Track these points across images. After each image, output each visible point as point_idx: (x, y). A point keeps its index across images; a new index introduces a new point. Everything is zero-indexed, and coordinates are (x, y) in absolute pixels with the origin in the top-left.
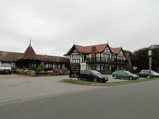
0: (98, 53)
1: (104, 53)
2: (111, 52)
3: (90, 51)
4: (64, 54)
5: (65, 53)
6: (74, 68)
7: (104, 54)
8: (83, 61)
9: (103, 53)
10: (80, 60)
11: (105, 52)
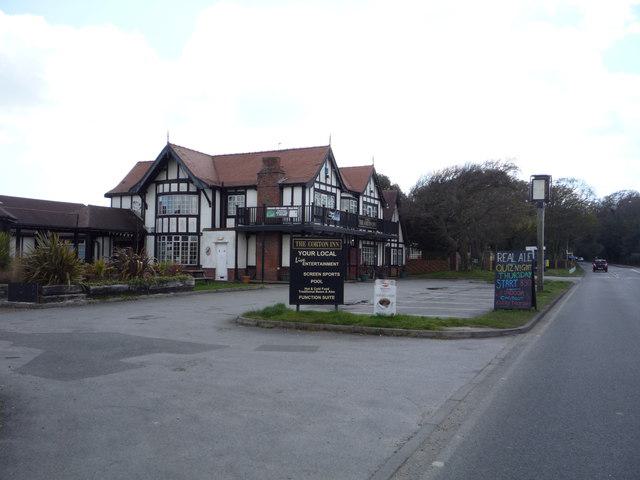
0: (293, 186)
1: (317, 186)
2: (341, 187)
3: (254, 180)
4: (107, 190)
5: (112, 184)
6: (313, 253)
7: (315, 190)
8: (218, 225)
9: (312, 189)
10: (198, 217)
11: (320, 183)
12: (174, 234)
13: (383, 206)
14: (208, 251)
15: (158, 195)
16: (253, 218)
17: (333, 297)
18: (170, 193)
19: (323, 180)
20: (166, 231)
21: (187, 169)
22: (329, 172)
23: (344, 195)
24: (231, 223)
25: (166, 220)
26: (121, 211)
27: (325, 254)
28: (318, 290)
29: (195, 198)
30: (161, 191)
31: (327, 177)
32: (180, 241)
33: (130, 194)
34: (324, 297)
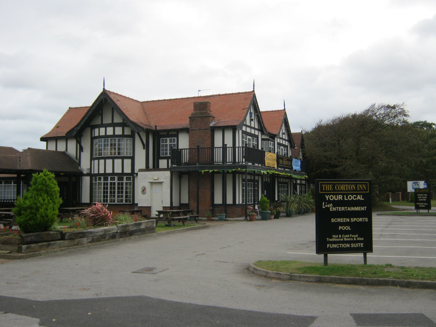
0: (223, 129)
2: (262, 129)
3: (186, 123)
6: (340, 197)
7: (243, 132)
8: (151, 166)
9: (240, 132)
10: (133, 159)
11: (247, 126)
12: (109, 174)
13: (292, 147)
14: (144, 191)
15: (93, 139)
16: (186, 158)
17: (362, 245)
18: (106, 136)
19: (248, 124)
20: (102, 171)
21: (121, 113)
22: (253, 115)
23: (264, 137)
24: (163, 163)
25: (102, 161)
26: (56, 152)
27: (352, 197)
28: (346, 238)
29: (129, 141)
30: (97, 134)
31: (251, 120)
32: (116, 181)
33: (67, 138)
34: (353, 245)
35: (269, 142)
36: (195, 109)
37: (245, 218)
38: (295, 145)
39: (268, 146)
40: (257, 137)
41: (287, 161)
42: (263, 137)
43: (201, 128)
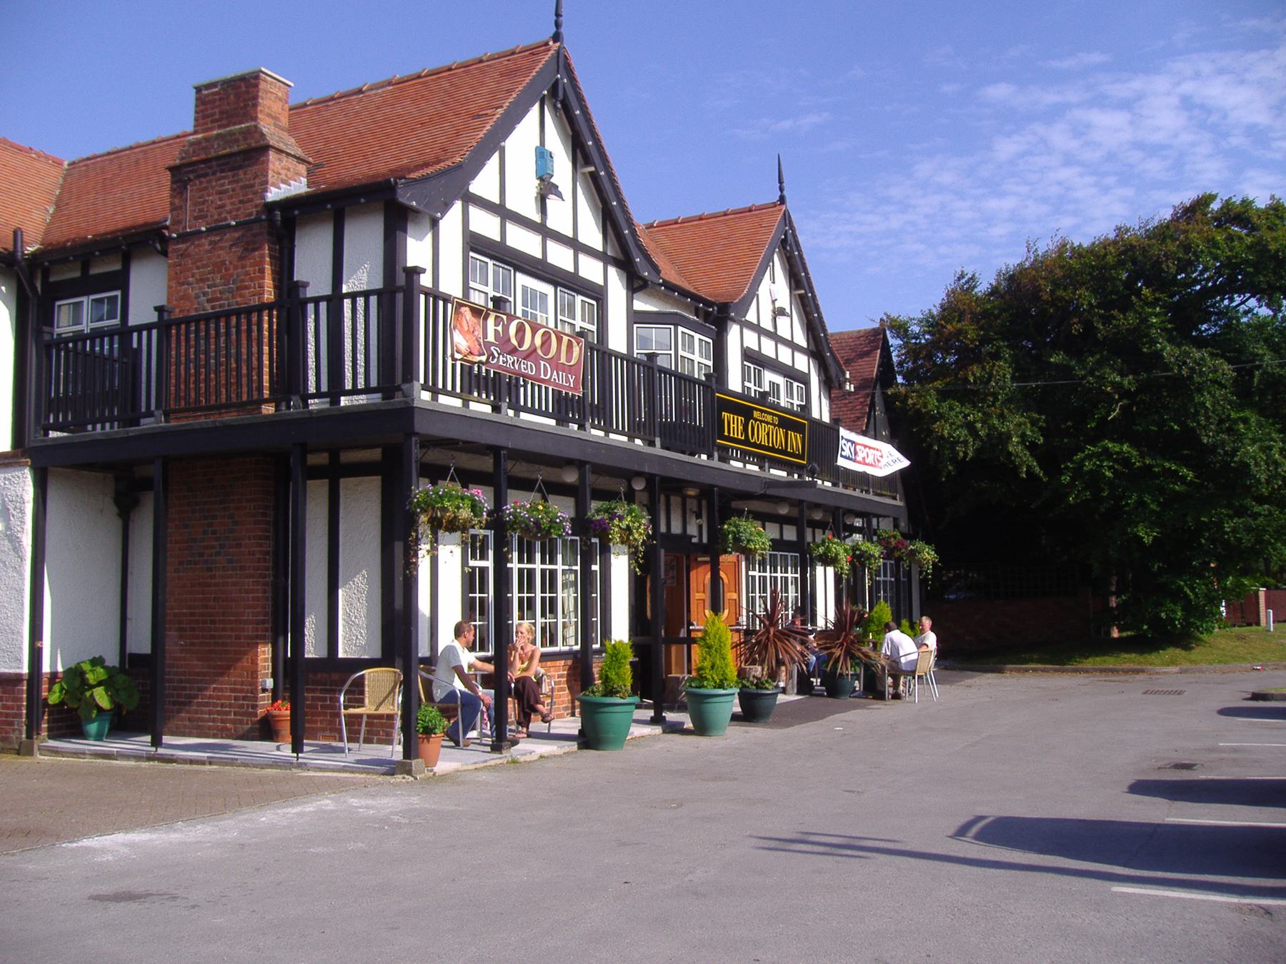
35: (681, 329)
36: (201, 121)
37: (653, 714)
38: (844, 374)
39: (672, 352)
40: (597, 294)
41: (779, 426)
42: (639, 305)
43: (226, 219)
